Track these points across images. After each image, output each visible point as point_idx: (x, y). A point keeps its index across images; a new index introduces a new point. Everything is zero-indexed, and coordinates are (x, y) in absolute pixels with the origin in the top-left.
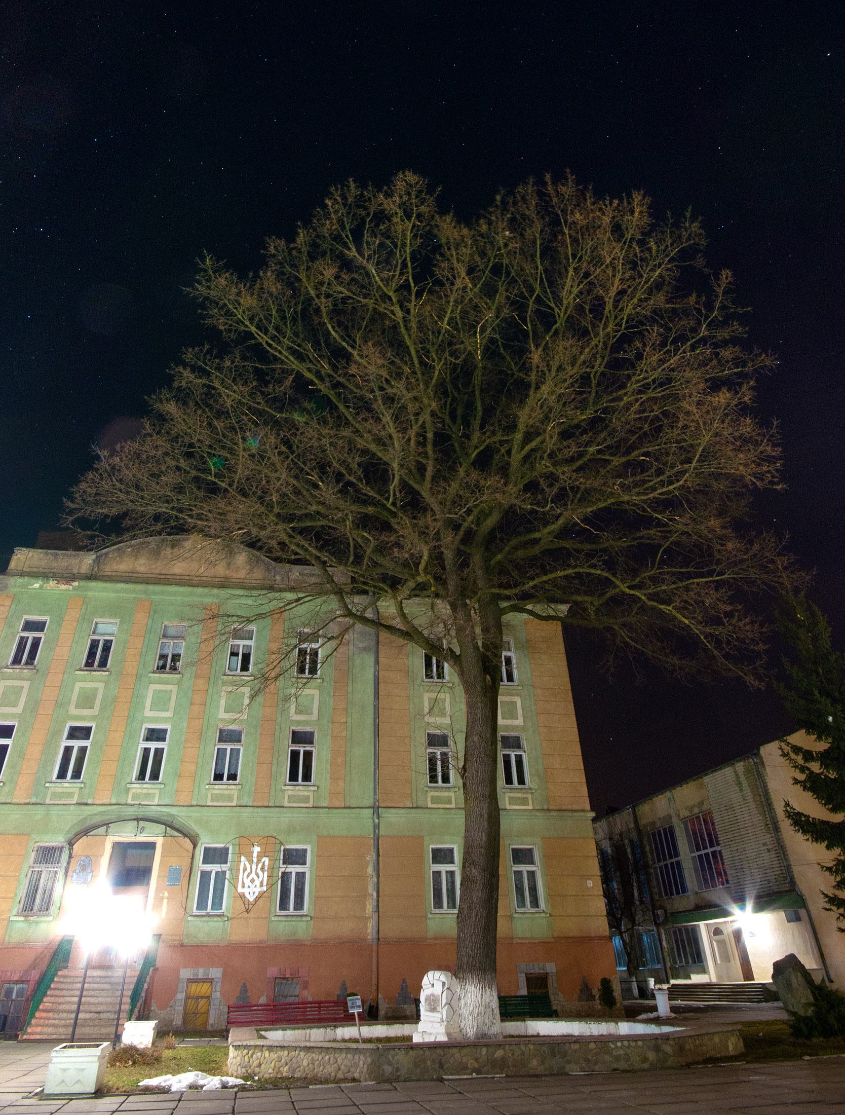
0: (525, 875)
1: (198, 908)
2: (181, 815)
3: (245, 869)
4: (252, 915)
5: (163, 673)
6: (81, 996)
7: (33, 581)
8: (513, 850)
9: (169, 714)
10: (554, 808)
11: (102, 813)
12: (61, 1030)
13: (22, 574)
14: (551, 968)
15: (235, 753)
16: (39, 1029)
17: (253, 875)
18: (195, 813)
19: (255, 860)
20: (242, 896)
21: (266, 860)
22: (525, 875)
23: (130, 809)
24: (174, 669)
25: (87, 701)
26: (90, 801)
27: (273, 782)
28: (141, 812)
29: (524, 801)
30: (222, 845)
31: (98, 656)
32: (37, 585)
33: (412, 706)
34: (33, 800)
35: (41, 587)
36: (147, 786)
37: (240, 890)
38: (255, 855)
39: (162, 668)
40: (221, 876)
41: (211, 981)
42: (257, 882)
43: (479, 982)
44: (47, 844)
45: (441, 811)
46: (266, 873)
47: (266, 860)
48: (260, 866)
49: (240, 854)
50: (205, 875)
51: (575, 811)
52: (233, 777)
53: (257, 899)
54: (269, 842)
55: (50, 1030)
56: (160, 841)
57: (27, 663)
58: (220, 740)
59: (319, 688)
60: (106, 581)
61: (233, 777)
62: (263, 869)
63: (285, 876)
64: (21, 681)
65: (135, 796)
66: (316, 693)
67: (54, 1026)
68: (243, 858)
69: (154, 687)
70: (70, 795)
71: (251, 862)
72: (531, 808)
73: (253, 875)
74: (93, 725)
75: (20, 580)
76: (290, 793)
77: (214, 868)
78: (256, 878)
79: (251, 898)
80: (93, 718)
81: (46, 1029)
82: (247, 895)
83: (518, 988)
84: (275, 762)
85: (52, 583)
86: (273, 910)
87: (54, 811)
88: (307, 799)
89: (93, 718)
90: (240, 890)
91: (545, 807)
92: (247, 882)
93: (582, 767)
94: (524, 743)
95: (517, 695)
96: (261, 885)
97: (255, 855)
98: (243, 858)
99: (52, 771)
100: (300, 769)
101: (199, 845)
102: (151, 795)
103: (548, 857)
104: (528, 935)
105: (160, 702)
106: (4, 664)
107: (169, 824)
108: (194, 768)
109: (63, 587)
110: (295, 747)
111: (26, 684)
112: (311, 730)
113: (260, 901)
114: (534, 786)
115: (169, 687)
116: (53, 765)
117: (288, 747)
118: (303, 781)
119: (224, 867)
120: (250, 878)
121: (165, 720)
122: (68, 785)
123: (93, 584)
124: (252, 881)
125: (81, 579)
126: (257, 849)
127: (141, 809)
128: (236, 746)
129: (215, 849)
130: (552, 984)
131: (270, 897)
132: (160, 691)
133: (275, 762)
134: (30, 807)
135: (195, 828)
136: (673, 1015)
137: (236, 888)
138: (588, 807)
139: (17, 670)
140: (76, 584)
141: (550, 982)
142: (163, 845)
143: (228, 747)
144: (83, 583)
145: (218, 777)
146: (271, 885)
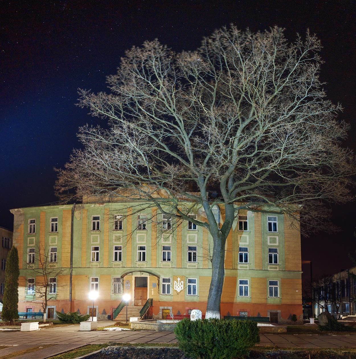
0: (273, 288)
1: (163, 293)
2: (154, 271)
3: (176, 284)
4: (179, 295)
5: (141, 230)
6: (127, 312)
7: (91, 205)
8: (270, 281)
9: (144, 242)
10: (287, 270)
11: (130, 269)
12: (124, 318)
13: (87, 203)
14: (279, 311)
15: (169, 253)
16: (118, 318)
17: (179, 286)
18: (158, 269)
19: (179, 282)
20: (176, 291)
21: (183, 282)
22: (273, 288)
23: (138, 268)
24: (144, 228)
25: (118, 239)
26: (125, 267)
27: (183, 261)
28: (141, 269)
29: (276, 268)
30: (168, 278)
31: (118, 226)
32: (93, 206)
33: (233, 239)
34: (109, 267)
35: (94, 206)
36: (142, 262)
37: (175, 289)
38: (179, 280)
39: (140, 229)
40: (168, 286)
41: (169, 309)
42: (180, 287)
43: (212, 312)
44: (117, 277)
45: (243, 270)
46: (183, 285)
47: (183, 282)
48: (181, 283)
49: (174, 280)
50: (164, 286)
51: (295, 271)
52: (169, 260)
53: (180, 292)
54: (183, 278)
55: (121, 318)
56: (148, 277)
57: (97, 230)
58: (164, 249)
59: (197, 233)
60: (115, 202)
61: (169, 260)
62: (181, 284)
63: (189, 286)
64: (95, 234)
65: (138, 265)
66: (196, 235)
67: (122, 318)
68: (175, 281)
69: (138, 234)
70: (119, 265)
71: (178, 282)
72: (278, 270)
73: (179, 286)
74: (122, 246)
75: (87, 205)
76: (189, 264)
77: (166, 284)
78: (179, 286)
79: (179, 291)
80: (121, 244)
81: (120, 318)
82: (177, 290)
83: (267, 315)
84: (183, 256)
85: (97, 205)
86: (186, 294)
87: (116, 269)
88: (195, 266)
89: (121, 244)
90: (175, 289)
91: (284, 270)
92: (177, 287)
93: (301, 258)
94: (278, 251)
95: (277, 236)
96: (182, 288)
97: (179, 280)
98: (175, 281)
99: (113, 259)
100: (192, 257)
101: (161, 278)
102: (144, 265)
103: (282, 284)
104: (272, 303)
105: (141, 239)
106: (90, 230)
107: (150, 273)
108: (156, 258)
109: (101, 205)
110: (190, 251)
111: (99, 235)
112: (195, 246)
113: (182, 292)
114: (280, 264)
115: (143, 234)
116: (112, 257)
117: (187, 251)
118: (167, 293)
119: (169, 283)
120: (178, 286)
121: (144, 244)
122: (118, 262)
123: (110, 204)
124: (179, 287)
125: (106, 203)
126: (179, 279)
127: (141, 268)
128: (169, 251)
129: (167, 279)
130: (279, 315)
131: (185, 291)
132: (140, 236)
133: (183, 256)
134: (108, 268)
135: (158, 273)
136: (315, 324)
137: (174, 288)
138: (301, 270)
139: (94, 232)
140: (105, 204)
141: (278, 314)
142: (150, 278)
143: (167, 251)
144: (107, 204)
145: (164, 260)
146: (185, 288)
